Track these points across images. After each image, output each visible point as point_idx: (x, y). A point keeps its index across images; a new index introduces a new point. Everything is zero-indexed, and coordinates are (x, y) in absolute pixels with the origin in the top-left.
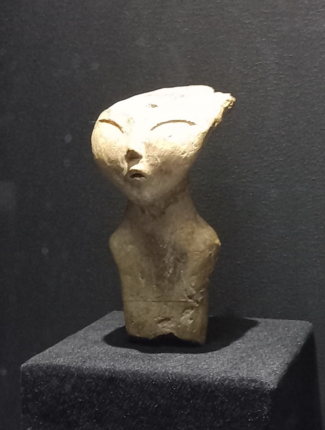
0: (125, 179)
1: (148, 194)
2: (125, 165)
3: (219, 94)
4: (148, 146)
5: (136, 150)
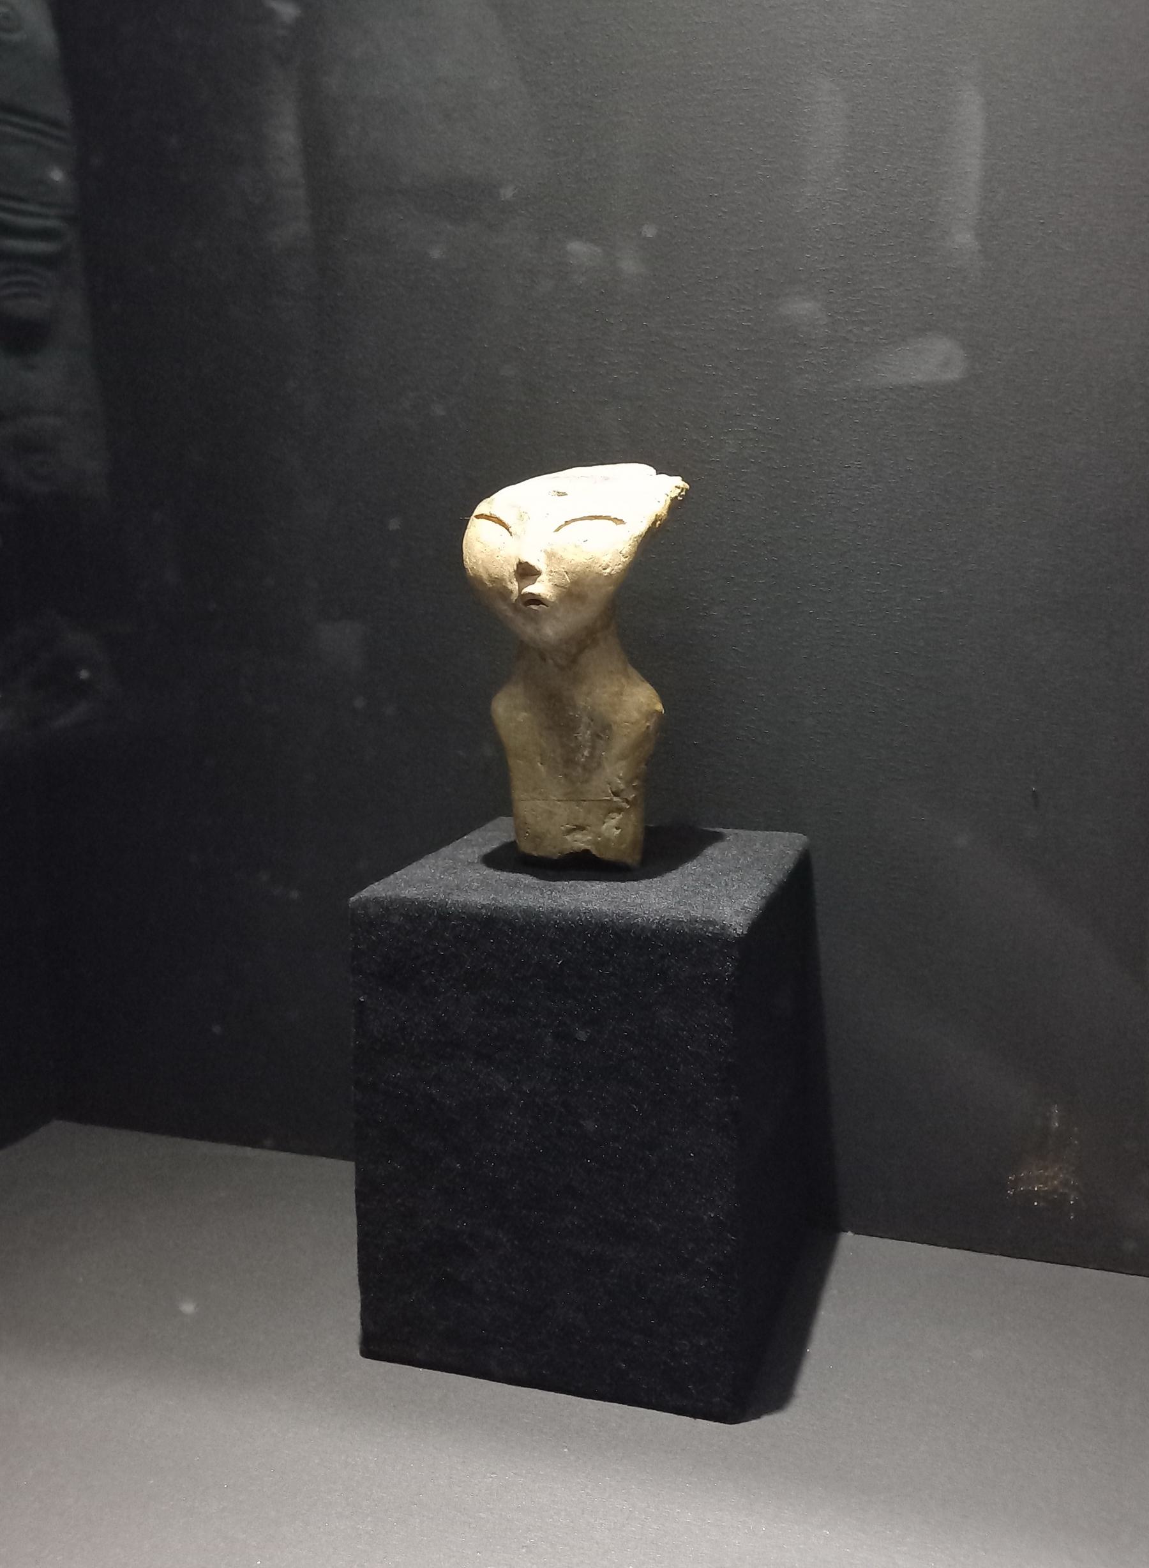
0: (515, 607)
1: (551, 631)
2: (514, 586)
4: (551, 556)
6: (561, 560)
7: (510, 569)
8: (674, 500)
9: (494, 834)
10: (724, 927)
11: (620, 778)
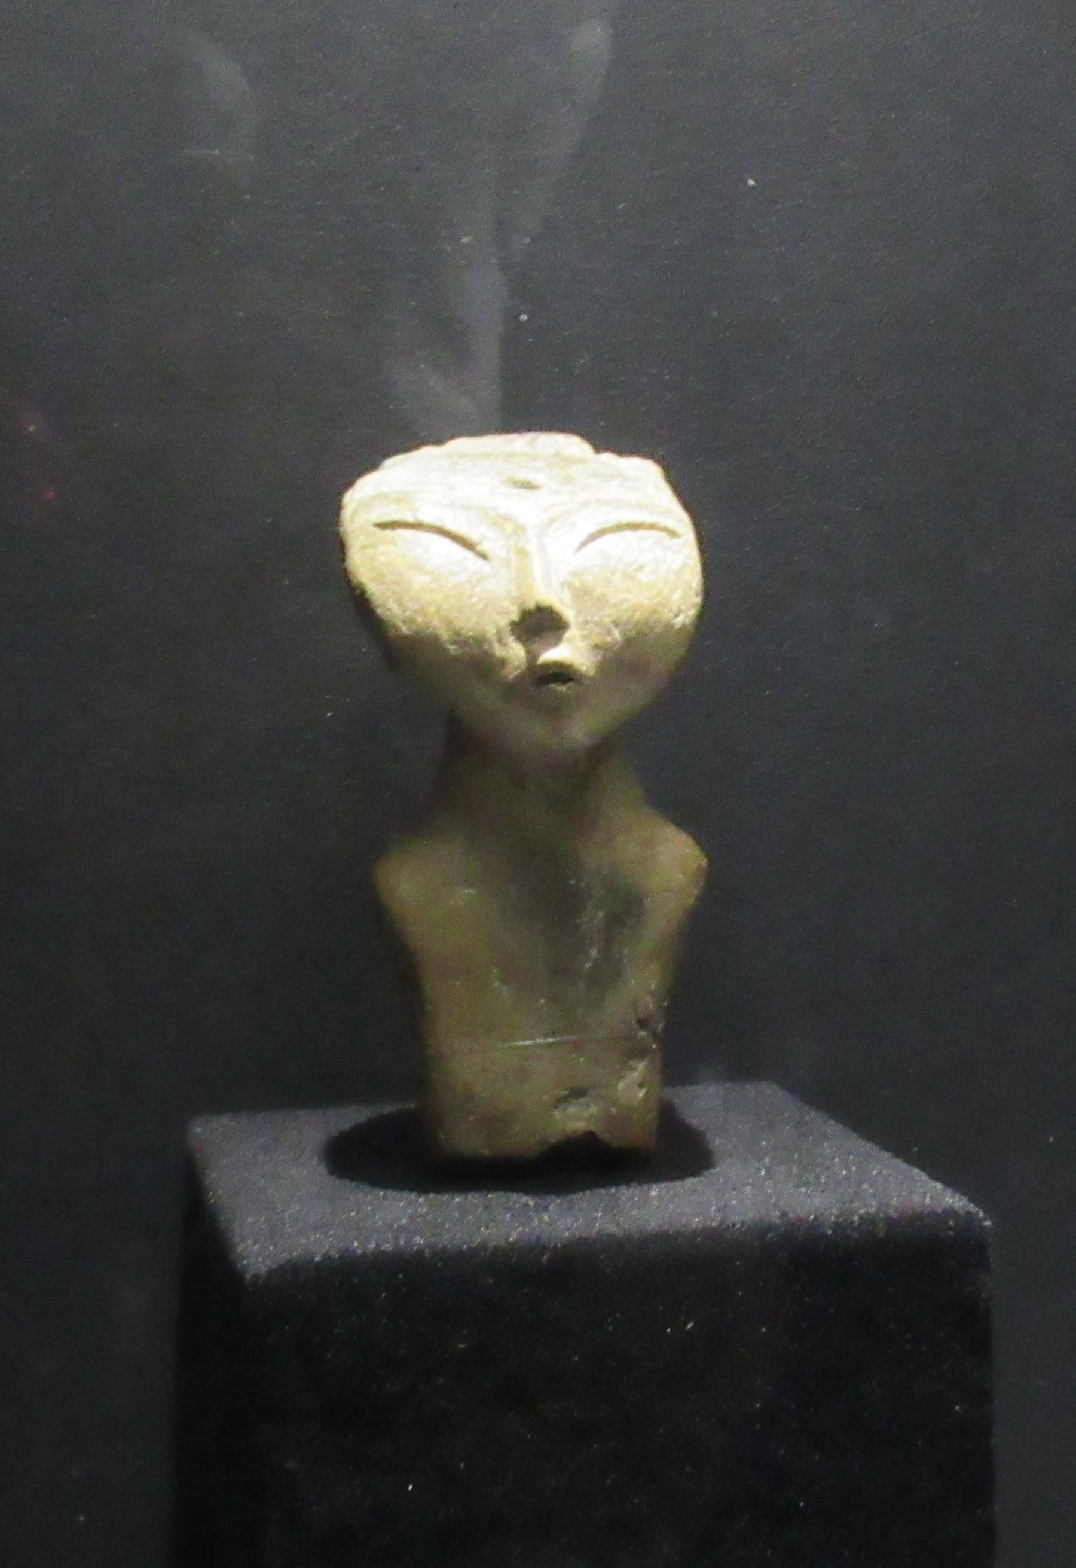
0: (513, 690)
1: (580, 729)
2: (515, 653)
4: (581, 594)
6: (602, 601)
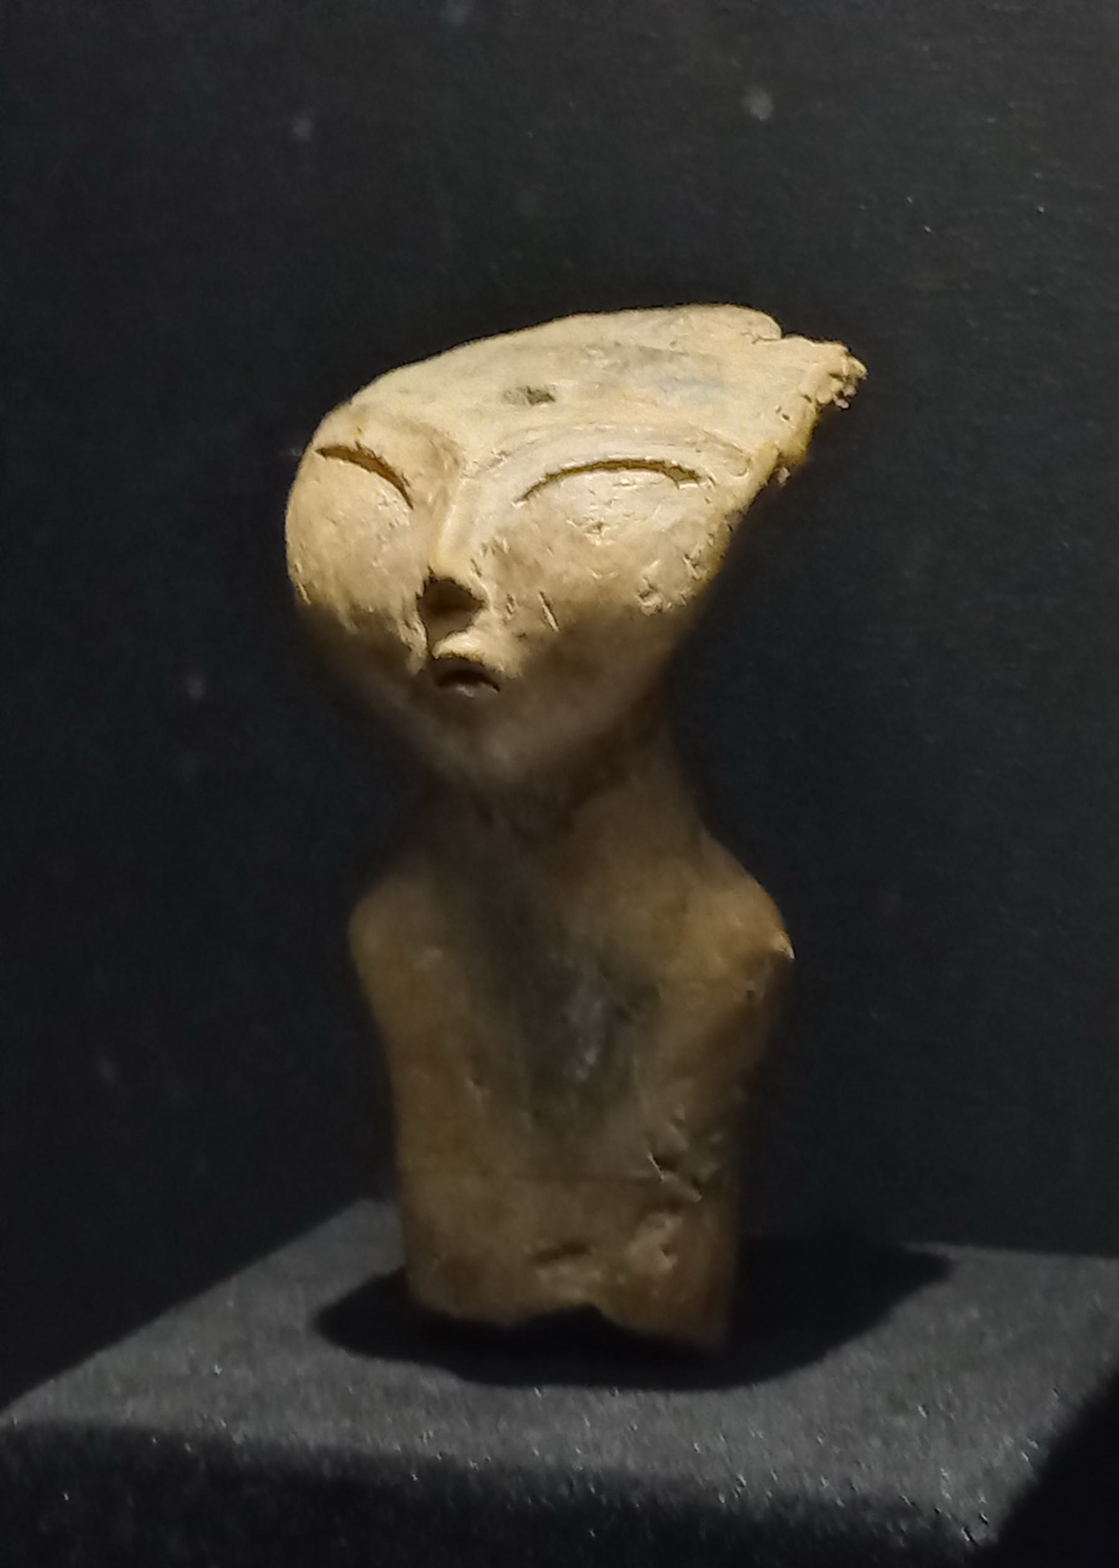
0: (416, 688)
1: (506, 750)
2: (416, 635)
3: (799, 343)
5: (465, 575)
6: (535, 571)
7: (400, 595)
8: (826, 411)
9: (347, 1250)
10: (938, 1521)
11: (678, 1123)
